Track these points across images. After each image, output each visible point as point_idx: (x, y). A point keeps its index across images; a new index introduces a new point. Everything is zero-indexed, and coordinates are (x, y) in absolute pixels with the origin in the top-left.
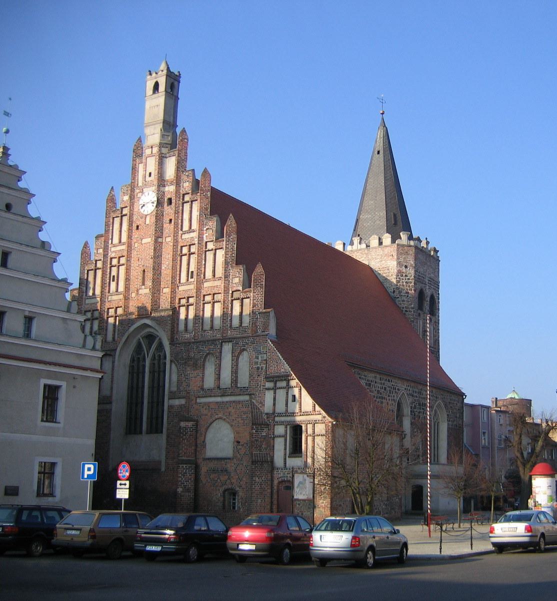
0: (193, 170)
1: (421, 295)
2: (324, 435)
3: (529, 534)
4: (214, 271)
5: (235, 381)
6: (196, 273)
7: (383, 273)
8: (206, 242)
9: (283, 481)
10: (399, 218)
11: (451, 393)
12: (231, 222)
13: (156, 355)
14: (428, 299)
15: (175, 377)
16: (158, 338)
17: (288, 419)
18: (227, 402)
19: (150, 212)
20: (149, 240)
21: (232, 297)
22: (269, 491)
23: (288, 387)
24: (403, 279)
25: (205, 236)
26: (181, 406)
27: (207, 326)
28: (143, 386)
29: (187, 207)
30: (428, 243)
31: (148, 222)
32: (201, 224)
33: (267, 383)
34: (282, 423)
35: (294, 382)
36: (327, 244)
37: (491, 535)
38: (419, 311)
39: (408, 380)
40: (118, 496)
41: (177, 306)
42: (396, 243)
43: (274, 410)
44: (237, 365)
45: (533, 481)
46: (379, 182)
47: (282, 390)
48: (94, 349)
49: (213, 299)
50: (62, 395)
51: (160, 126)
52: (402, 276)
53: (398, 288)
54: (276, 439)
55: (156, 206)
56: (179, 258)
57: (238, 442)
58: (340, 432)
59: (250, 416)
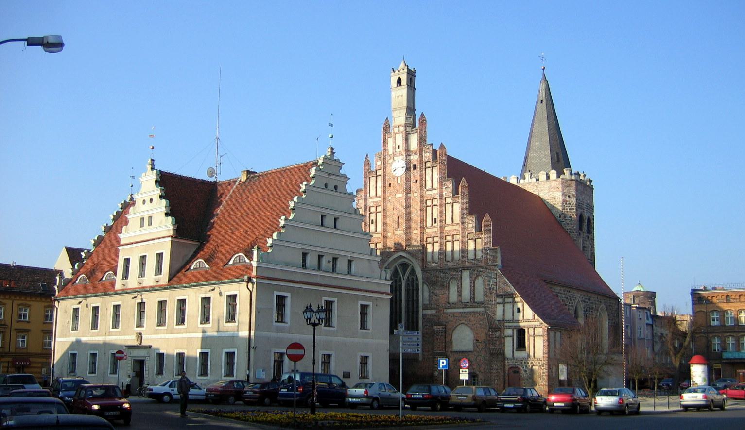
0: (432, 144)
1: (581, 218)
2: (542, 336)
3: (705, 400)
4: (453, 219)
5: (473, 297)
6: (439, 219)
7: (551, 202)
8: (445, 198)
9: (512, 367)
10: (561, 156)
11: (610, 298)
12: (463, 183)
13: (410, 278)
14: (586, 221)
15: (426, 294)
16: (411, 266)
17: (515, 324)
18: (468, 312)
19: (401, 175)
20: (401, 195)
21: (468, 237)
22: (503, 374)
23: (514, 302)
24: (567, 207)
25: (444, 193)
26: (432, 315)
27: (449, 258)
28: (401, 300)
29: (429, 171)
30: (585, 176)
31: (399, 182)
32: (441, 184)
33: (497, 299)
34: (509, 327)
35: (518, 299)
36: (502, 178)
37: (681, 400)
38: (580, 231)
39: (581, 290)
40: (461, 378)
41: (425, 243)
42: (561, 177)
43: (513, 318)
44: (474, 286)
45: (691, 368)
46: (543, 127)
47: (509, 304)
48: (386, 279)
49: (453, 239)
50: (370, 311)
51: (405, 111)
52: (566, 204)
53: (563, 214)
54: (506, 338)
55: (406, 171)
56: (425, 208)
57: (477, 340)
58: (552, 333)
59: (487, 322)
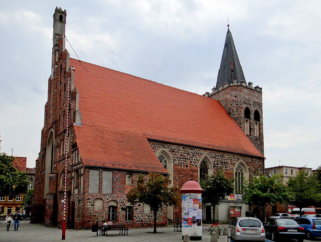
52: (233, 102)
